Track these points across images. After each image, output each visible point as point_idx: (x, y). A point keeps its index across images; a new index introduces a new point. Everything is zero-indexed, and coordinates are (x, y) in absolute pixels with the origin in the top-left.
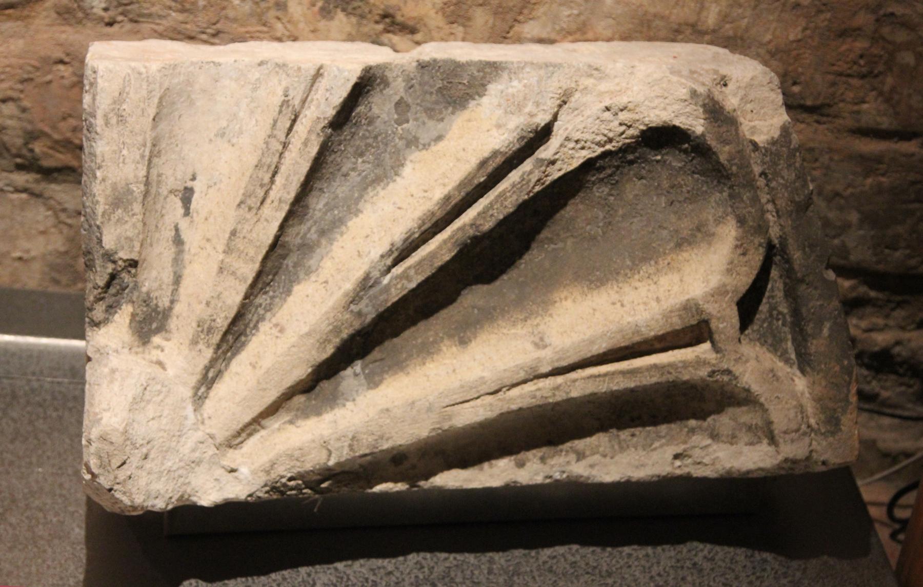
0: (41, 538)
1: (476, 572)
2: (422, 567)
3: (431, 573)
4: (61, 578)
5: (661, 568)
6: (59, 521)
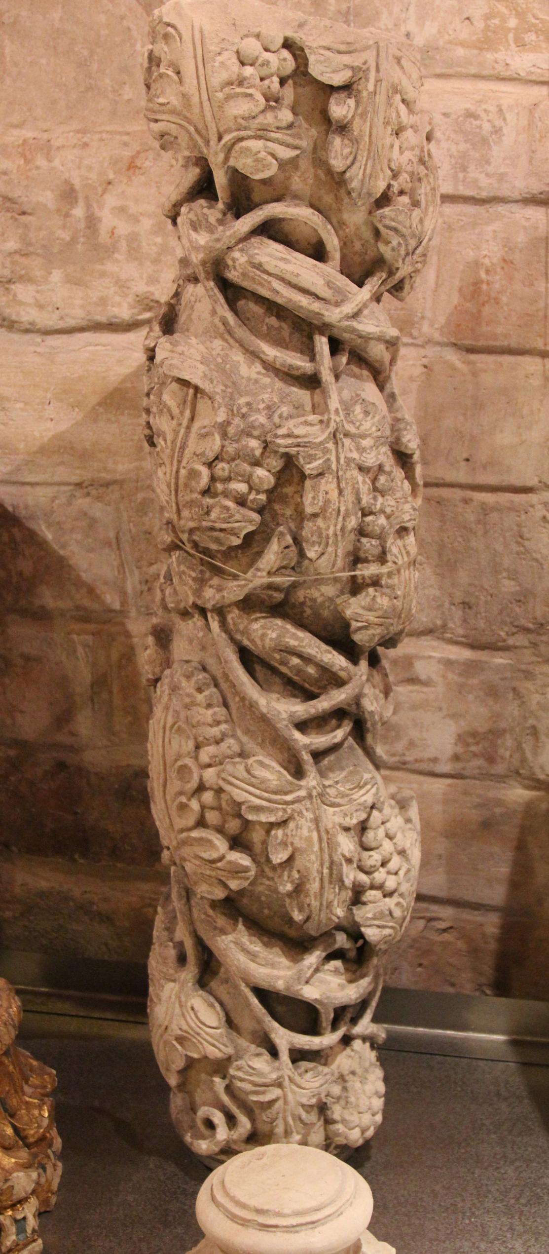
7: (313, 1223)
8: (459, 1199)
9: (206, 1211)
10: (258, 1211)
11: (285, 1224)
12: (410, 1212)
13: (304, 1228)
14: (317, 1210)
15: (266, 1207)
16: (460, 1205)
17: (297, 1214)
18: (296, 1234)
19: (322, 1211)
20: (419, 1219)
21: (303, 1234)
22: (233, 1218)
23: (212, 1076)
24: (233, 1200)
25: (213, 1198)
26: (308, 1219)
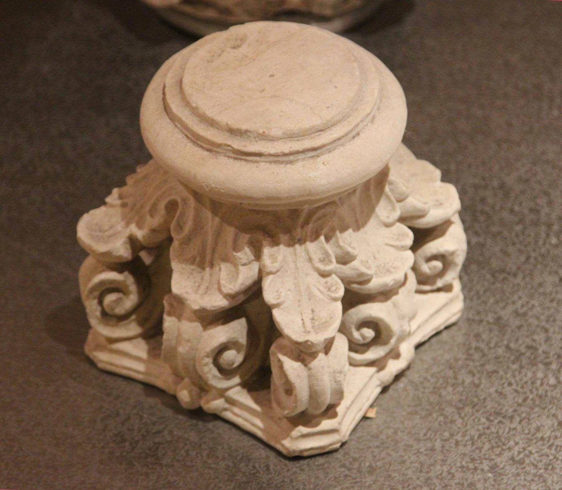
0: (450, 403)
1: (193, 453)
2: (123, 440)
3: (133, 448)
4: (473, 460)
5: (445, 469)
6: (473, 383)
7: (314, 149)
8: (542, 201)
9: (156, 126)
10: (233, 132)
11: (272, 151)
12: (457, 360)
13: (300, 156)
14: (321, 130)
15: (244, 127)
16: (545, 210)
17: (291, 136)
18: (289, 166)
19: (328, 132)
20: (471, 373)
21: (299, 165)
22: (196, 139)
23: (147, 268)
24: (195, 111)
25: (166, 108)
26: (308, 143)
